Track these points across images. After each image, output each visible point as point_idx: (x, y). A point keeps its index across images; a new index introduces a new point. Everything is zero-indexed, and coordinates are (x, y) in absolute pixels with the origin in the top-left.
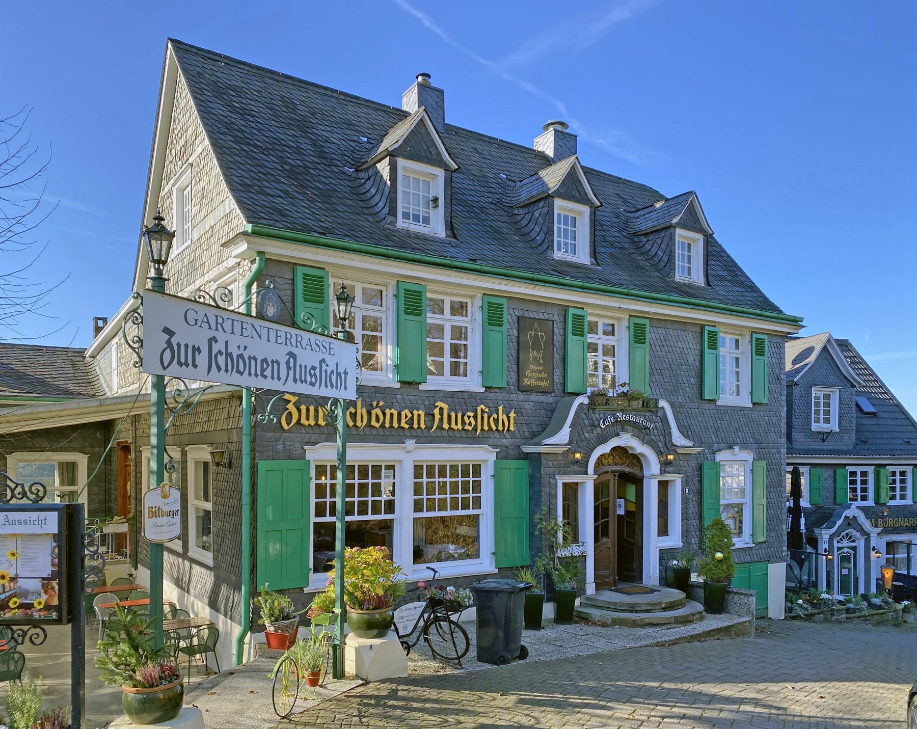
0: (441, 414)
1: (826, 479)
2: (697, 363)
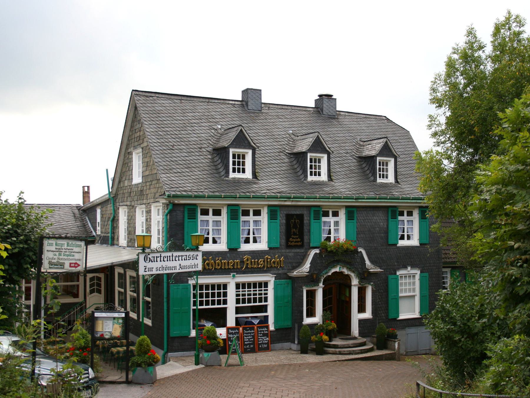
2: (385, 226)
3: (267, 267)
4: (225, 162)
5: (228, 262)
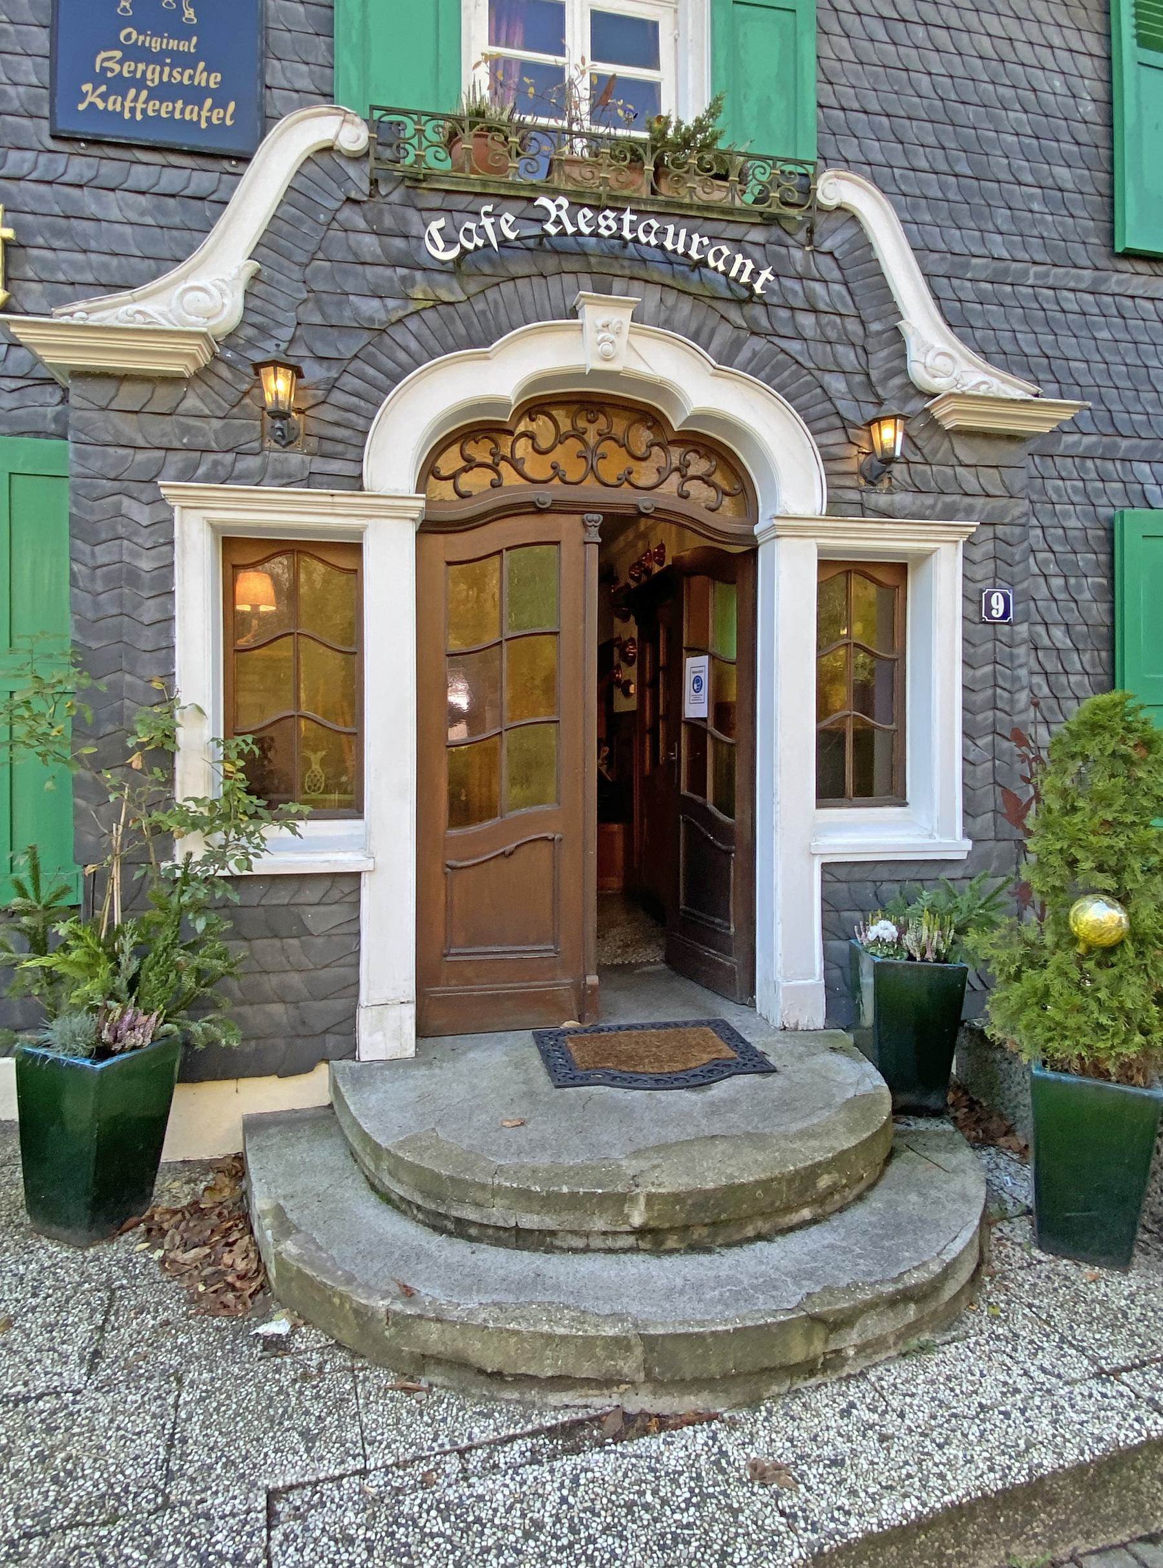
2: (1088, 109)
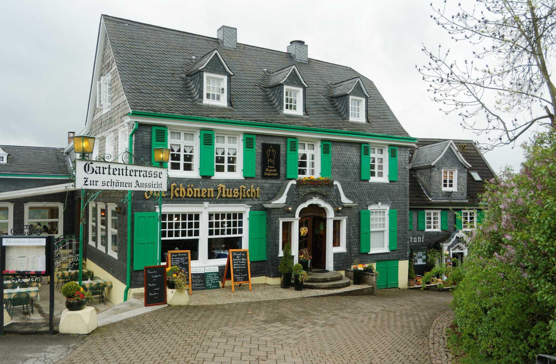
0: (222, 190)
1: (450, 217)
2: (358, 162)
3: (243, 197)
4: (199, 87)
5: (201, 191)
